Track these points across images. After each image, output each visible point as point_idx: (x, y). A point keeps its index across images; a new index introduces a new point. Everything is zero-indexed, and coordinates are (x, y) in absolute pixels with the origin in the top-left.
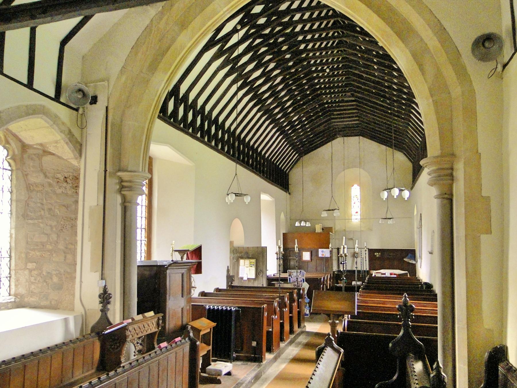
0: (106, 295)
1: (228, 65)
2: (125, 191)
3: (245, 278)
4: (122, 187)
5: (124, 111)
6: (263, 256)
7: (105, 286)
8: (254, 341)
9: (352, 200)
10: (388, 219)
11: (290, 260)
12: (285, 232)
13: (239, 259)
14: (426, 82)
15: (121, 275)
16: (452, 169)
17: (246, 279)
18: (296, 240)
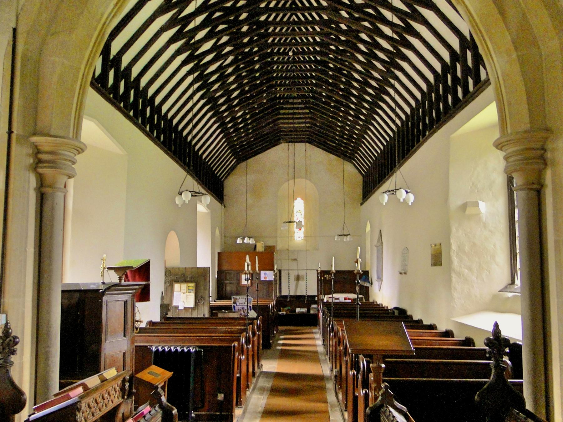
0: (8, 340)
1: (174, 26)
2: (41, 167)
3: (181, 308)
4: (38, 162)
5: (44, 40)
6: (205, 279)
7: (7, 324)
8: (221, 393)
9: (295, 215)
10: (345, 235)
11: (226, 284)
12: (219, 251)
13: (174, 283)
14: (508, 29)
15: (547, 263)
16: (544, 149)
17: (183, 308)
18: (257, 257)
